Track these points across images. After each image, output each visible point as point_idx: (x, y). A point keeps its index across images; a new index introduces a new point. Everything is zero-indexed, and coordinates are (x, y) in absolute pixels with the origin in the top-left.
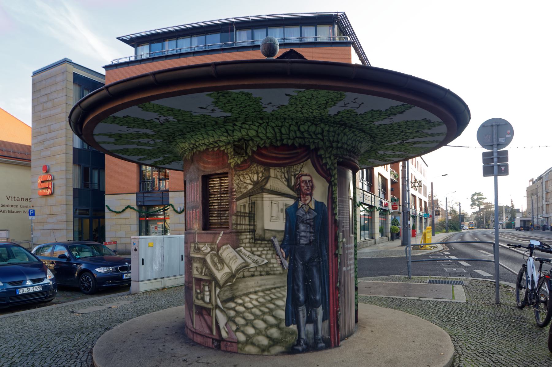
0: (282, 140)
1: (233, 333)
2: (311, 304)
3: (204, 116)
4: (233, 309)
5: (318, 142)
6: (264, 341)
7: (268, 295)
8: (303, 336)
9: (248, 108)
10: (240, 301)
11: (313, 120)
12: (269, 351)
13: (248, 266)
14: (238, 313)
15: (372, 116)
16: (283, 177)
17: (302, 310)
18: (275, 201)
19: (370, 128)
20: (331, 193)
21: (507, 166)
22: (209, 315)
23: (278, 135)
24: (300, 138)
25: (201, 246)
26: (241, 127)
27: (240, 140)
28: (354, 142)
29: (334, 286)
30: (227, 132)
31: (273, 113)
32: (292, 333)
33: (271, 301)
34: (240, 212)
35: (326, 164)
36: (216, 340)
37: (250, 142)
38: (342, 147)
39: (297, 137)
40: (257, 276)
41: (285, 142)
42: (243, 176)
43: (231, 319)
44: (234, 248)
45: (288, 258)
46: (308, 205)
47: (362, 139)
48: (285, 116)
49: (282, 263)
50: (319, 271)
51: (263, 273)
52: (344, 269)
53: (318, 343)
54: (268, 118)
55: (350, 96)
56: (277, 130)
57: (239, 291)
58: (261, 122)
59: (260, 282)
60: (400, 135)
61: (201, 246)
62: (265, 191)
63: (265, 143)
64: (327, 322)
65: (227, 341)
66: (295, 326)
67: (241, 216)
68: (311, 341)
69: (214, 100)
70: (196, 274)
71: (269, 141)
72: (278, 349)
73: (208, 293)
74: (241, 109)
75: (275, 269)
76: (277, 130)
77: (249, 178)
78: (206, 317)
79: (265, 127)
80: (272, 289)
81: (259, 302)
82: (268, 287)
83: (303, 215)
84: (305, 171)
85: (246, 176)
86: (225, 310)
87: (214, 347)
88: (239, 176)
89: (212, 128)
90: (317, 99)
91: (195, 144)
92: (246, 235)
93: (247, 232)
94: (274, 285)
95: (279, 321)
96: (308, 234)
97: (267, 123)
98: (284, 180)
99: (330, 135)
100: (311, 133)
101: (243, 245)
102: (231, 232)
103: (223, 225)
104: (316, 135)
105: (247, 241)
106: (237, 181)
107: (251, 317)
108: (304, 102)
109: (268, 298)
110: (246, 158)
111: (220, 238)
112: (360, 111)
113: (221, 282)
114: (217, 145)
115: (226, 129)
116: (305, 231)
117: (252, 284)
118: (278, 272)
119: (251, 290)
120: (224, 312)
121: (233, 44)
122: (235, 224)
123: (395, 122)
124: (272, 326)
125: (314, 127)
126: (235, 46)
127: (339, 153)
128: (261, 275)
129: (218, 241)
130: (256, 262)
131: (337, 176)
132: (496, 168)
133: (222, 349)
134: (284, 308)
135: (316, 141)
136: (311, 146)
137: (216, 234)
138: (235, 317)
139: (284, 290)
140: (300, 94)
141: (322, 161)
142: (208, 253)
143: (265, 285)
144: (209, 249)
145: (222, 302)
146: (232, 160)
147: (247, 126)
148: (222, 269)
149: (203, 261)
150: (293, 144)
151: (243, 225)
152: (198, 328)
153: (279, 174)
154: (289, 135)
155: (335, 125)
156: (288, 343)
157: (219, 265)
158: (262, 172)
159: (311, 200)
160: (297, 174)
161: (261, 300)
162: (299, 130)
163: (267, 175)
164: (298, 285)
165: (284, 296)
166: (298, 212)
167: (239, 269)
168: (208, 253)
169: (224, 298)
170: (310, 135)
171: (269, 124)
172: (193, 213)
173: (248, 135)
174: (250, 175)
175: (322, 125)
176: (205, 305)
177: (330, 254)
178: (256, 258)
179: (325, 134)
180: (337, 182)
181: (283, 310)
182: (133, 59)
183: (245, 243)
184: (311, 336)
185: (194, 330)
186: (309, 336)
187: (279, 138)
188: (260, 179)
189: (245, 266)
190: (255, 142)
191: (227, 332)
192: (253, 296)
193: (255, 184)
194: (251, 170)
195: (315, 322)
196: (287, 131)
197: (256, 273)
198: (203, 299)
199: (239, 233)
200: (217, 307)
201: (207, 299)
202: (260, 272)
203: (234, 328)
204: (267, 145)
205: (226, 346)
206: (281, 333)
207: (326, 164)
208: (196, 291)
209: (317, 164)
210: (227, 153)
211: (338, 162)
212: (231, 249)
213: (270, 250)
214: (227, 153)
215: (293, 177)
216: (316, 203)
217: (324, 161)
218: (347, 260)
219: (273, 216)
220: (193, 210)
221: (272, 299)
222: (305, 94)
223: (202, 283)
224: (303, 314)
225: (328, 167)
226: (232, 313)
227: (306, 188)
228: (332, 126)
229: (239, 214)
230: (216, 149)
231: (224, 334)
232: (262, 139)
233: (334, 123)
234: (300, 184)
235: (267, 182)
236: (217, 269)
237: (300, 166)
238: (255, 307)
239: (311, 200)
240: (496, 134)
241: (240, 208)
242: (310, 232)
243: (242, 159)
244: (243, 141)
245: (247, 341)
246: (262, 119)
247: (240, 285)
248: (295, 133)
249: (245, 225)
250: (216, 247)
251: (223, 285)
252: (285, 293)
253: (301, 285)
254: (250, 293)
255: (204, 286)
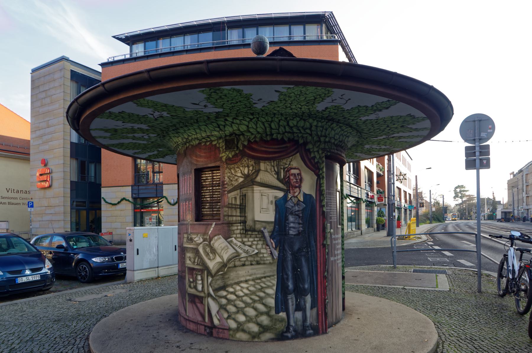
0: (272, 135)
1: (224, 321)
2: (300, 292)
3: (197, 111)
4: (225, 297)
5: (307, 137)
6: (255, 328)
7: (258, 283)
8: (292, 323)
9: (239, 104)
10: (231, 290)
11: (302, 116)
12: (259, 338)
13: (239, 255)
14: (229, 301)
15: (359, 112)
16: (273, 170)
17: (291, 298)
18: (265, 193)
19: (357, 123)
20: (319, 186)
21: (488, 160)
22: (202, 303)
23: (268, 129)
24: (289, 132)
25: (193, 236)
26: (233, 123)
27: (231, 135)
28: (341, 137)
29: (322, 275)
30: (219, 127)
31: (263, 108)
32: (282, 320)
33: (261, 289)
34: (232, 204)
35: (314, 158)
36: (208, 327)
37: (241, 137)
38: (329, 142)
39: (286, 132)
40: (247, 265)
41: (274, 136)
42: (234, 170)
43: (222, 307)
44: (226, 239)
45: (278, 248)
46: (296, 197)
47: (349, 134)
48: (275, 112)
49: (271, 253)
50: (307, 260)
51: (254, 263)
52: (332, 259)
53: (306, 330)
54: (259, 114)
55: (337, 92)
56: (267, 125)
57: (230, 280)
58: (251, 117)
59: (251, 272)
60: (386, 130)
61: (193, 236)
62: (255, 183)
63: (255, 137)
64: (315, 310)
65: (219, 328)
66: (285, 313)
67: (232, 208)
68: (300, 328)
69: (206, 96)
70: (188, 263)
71: (259, 135)
72: (268, 335)
73: (200, 282)
74: (233, 105)
75: (265, 259)
76: (267, 125)
77: (240, 172)
78: (199, 305)
79: (255, 123)
80: (262, 278)
81: (250, 291)
82: (258, 276)
83: (292, 207)
84: (294, 164)
85: (237, 169)
86: (217, 298)
87: (206, 334)
88: (230, 169)
89: (204, 123)
90: (305, 96)
91: (188, 138)
92: (237, 226)
93: (239, 223)
94: (264, 274)
95: (269, 309)
96: (297, 226)
97: (258, 118)
98: (273, 173)
99: (319, 130)
100: (300, 128)
101: (235, 236)
102: (223, 224)
103: (215, 217)
104: (305, 130)
105: (238, 231)
106: (229, 174)
107: (242, 305)
108: (293, 98)
109: (258, 287)
110: (237, 152)
111: (212, 229)
112: (347, 107)
113: (213, 272)
114: (209, 140)
115: (217, 124)
116: (294, 223)
117: (243, 273)
118: (268, 262)
119: (242, 279)
120: (216, 300)
121: (225, 42)
122: (226, 216)
123: (381, 117)
124: (262, 314)
125: (303, 122)
126: (226, 44)
127: (327, 147)
128: (252, 265)
129: (210, 232)
130: (247, 252)
131: (324, 170)
132: (478, 162)
133: (214, 335)
134: (274, 296)
135: (305, 136)
136: (300, 140)
137: (208, 225)
138: (226, 305)
139: (273, 279)
140: (289, 91)
141: (310, 155)
142: (201, 243)
143: (255, 274)
144: (201, 240)
145: (214, 291)
146: (223, 154)
147: (238, 121)
148: (214, 259)
149: (196, 251)
150: (282, 138)
151: (234, 216)
152: (191, 315)
153: (269, 168)
154: (278, 130)
155: (323, 120)
156: (278, 330)
157: (211, 255)
158: (252, 165)
159: (300, 193)
160: (287, 167)
161: (252, 288)
162: (288, 125)
163: (257, 169)
164: (287, 275)
165: (274, 285)
166: (287, 204)
167: (231, 259)
168: (201, 243)
169: (216, 286)
170: (299, 130)
171: (260, 119)
172: (186, 205)
173: (239, 130)
174: (241, 168)
175: (311, 120)
176: (198, 294)
177: (318, 245)
178: (247, 248)
179: (313, 128)
180: (324, 175)
181: (273, 298)
182: (128, 56)
183: (236, 234)
184: (300, 323)
185: (187, 318)
186: (298, 323)
187: (269, 133)
188: (250, 172)
189: (236, 256)
190: (246, 137)
191: (218, 320)
192: (244, 285)
193: (246, 177)
194: (242, 164)
195: (304, 310)
196: (277, 126)
197: (247, 263)
198: (195, 287)
199: (230, 224)
200: (209, 295)
201: (200, 288)
202: (251, 261)
203: (226, 315)
204: (257, 140)
205: (218, 332)
206: (271, 321)
207: (314, 158)
208: (189, 280)
209: (305, 158)
210: (219, 147)
211: (326, 156)
212: (223, 240)
213: (260, 240)
214: (219, 147)
215: (282, 171)
216: (305, 195)
217: (312, 155)
218: (334, 250)
219: (263, 208)
220: (186, 202)
221: (262, 288)
222: (294, 91)
223: (194, 273)
224: (292, 302)
225: (316, 160)
226: (224, 301)
227: (295, 180)
228: (320, 121)
229: (231, 206)
230: (208, 143)
231: (216, 322)
232: (252, 134)
233: (322, 118)
234: (289, 177)
235: (257, 175)
236: (210, 259)
237: (289, 160)
238: (246, 295)
239: (300, 193)
240: (478, 129)
241: (232, 200)
242: (299, 224)
243: (233, 153)
244: (234, 135)
245: (238, 328)
246: (252, 114)
247: (232, 274)
248: (285, 128)
249: (236, 216)
250: (208, 237)
251: (215, 274)
252: (275, 282)
253: (290, 274)
254: (241, 282)
255: (197, 275)
